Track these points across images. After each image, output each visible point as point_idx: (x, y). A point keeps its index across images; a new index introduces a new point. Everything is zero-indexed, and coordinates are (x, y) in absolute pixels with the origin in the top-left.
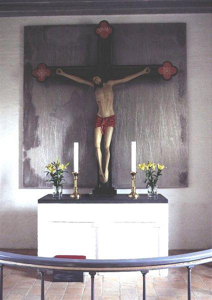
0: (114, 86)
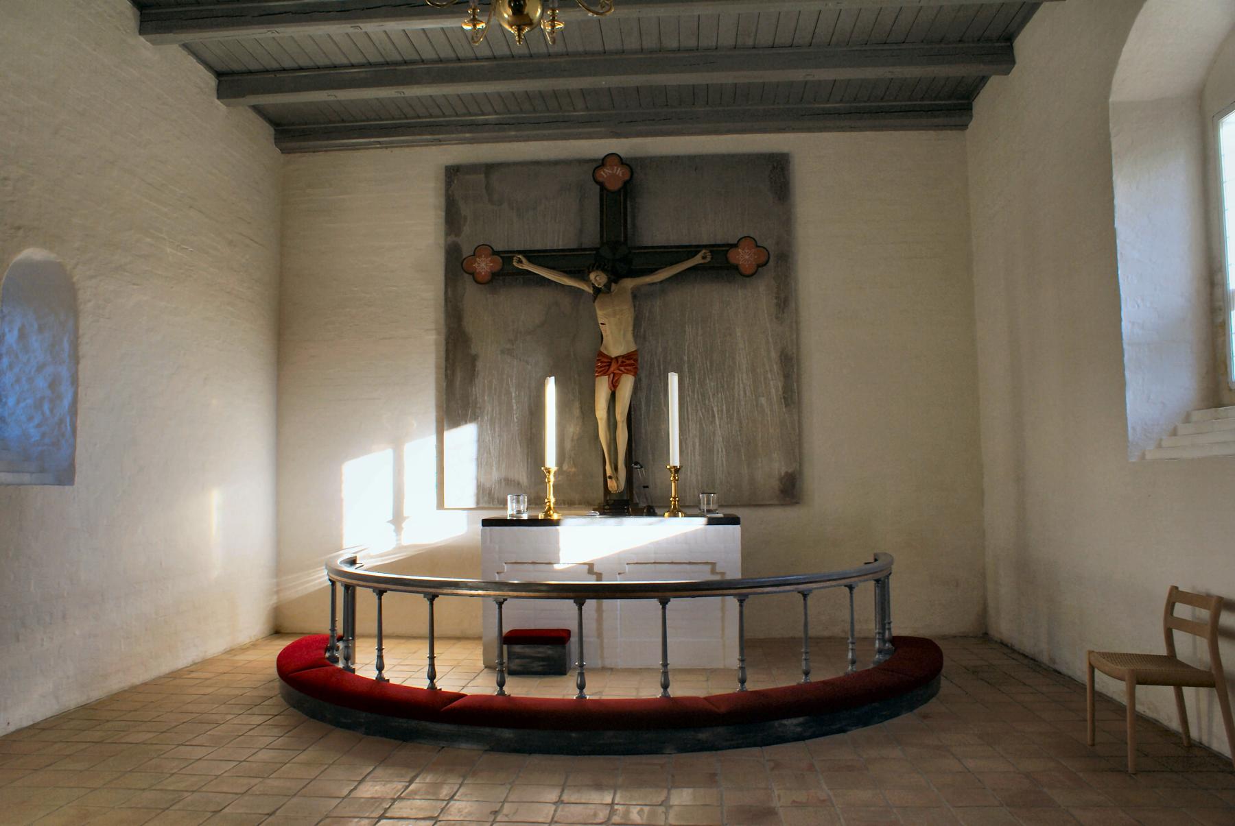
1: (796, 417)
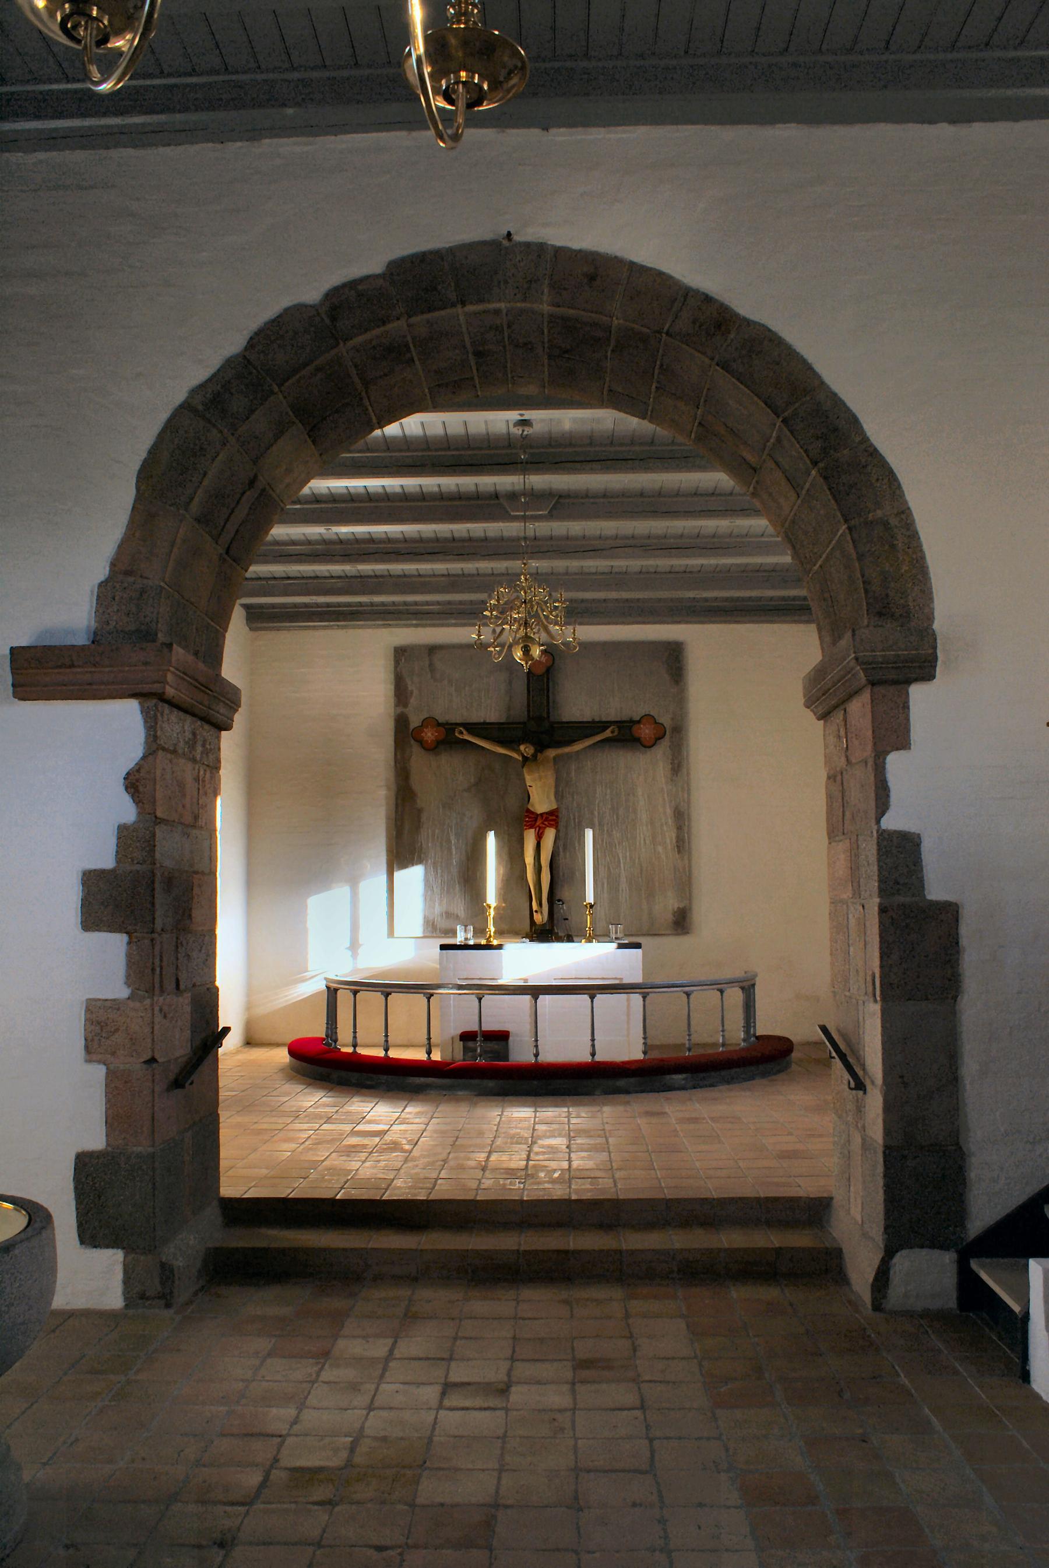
0: (555, 758)
1: (687, 862)
